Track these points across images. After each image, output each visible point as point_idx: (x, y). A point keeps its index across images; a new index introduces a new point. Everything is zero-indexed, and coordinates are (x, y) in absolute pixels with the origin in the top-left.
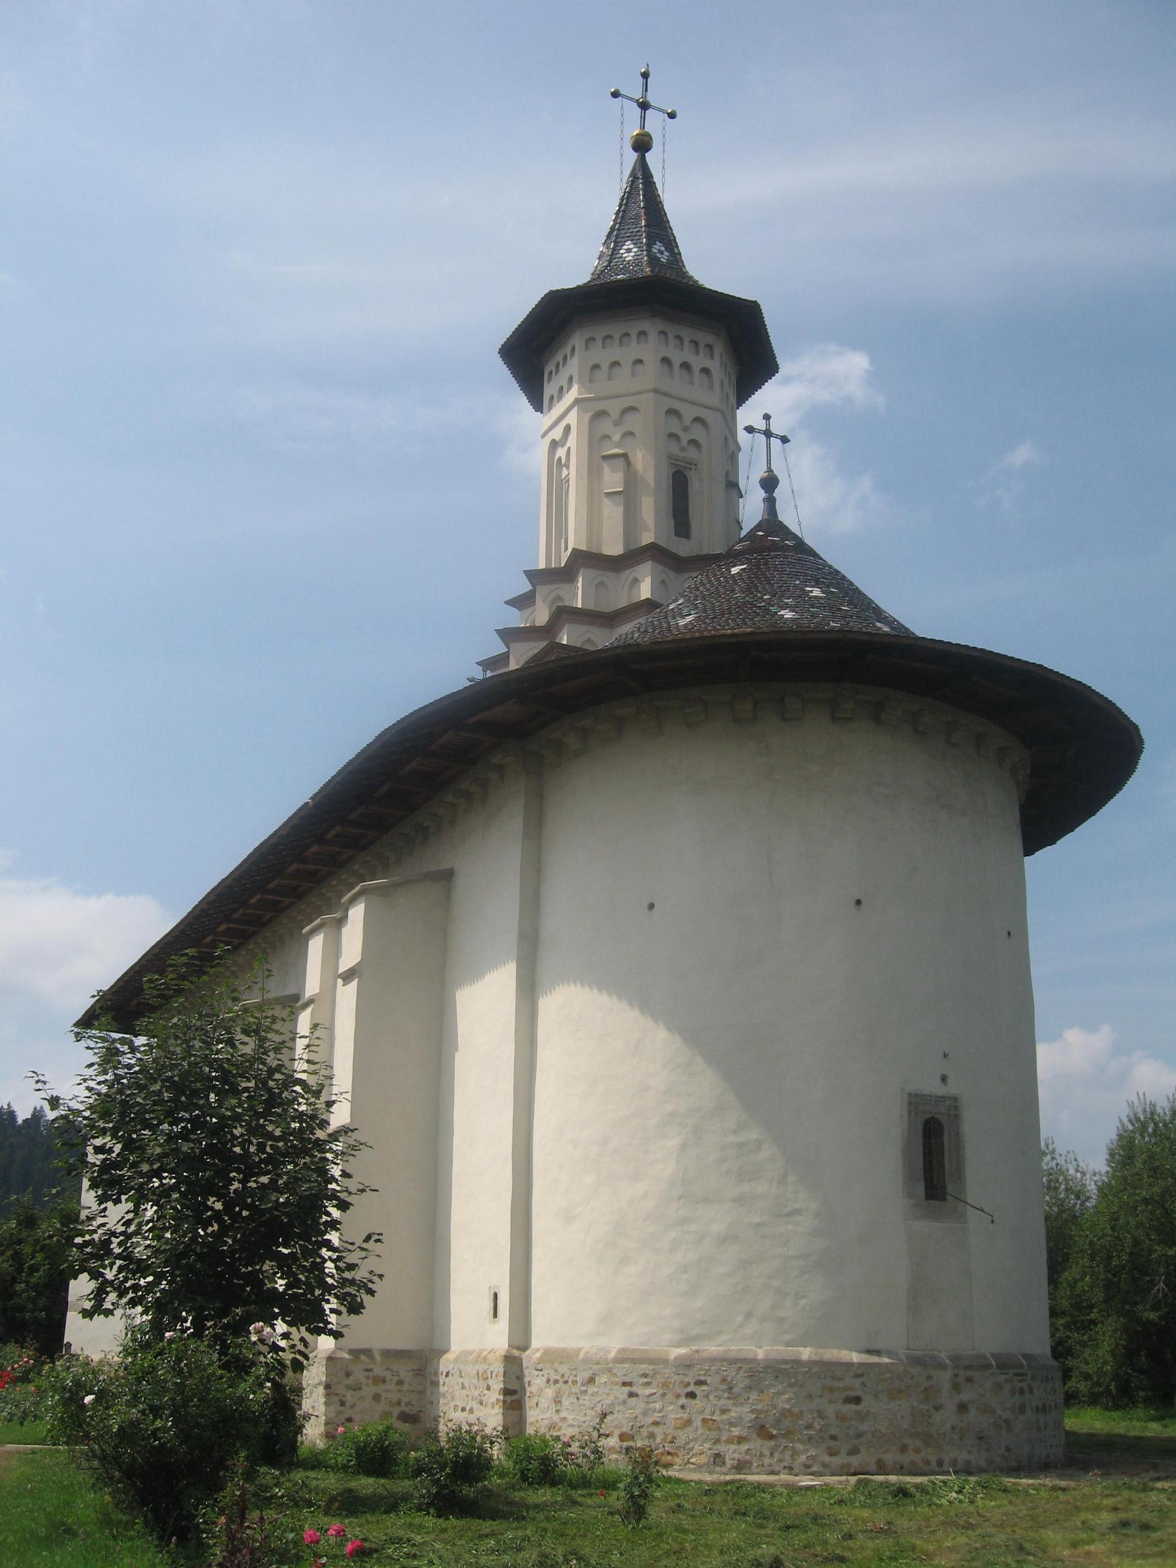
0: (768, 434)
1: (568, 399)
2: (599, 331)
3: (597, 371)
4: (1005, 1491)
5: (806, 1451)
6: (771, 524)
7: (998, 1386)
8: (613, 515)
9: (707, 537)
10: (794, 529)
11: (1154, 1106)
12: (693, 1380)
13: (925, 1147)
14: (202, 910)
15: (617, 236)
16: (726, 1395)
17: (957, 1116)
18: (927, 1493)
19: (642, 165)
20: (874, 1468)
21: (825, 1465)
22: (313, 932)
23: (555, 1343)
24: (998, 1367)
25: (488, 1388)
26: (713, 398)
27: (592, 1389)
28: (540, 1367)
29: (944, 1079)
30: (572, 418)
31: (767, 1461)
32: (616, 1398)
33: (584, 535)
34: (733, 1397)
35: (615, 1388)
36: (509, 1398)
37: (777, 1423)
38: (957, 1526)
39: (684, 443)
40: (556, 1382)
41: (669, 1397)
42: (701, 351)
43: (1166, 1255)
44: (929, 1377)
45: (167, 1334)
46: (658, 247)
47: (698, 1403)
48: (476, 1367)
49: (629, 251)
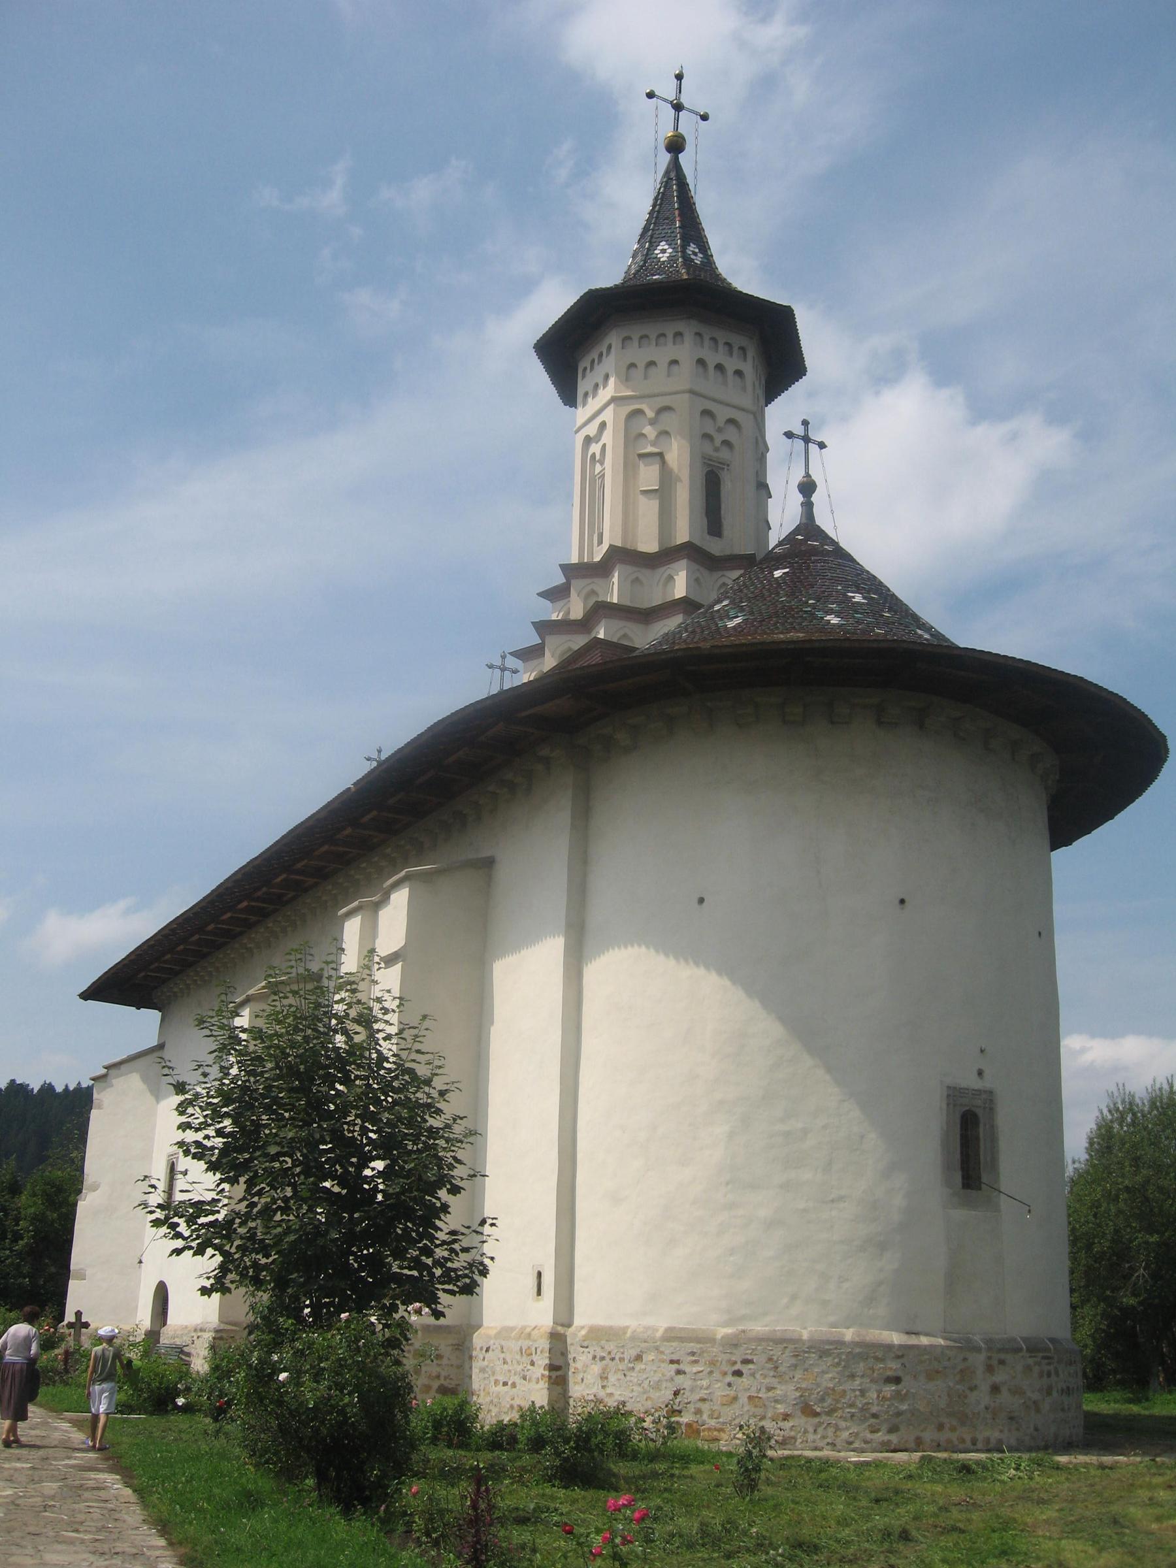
0: (807, 439)
1: (604, 396)
2: (636, 331)
3: (633, 370)
4: (1058, 1468)
5: (847, 1428)
6: (808, 527)
7: (1028, 1368)
8: (648, 510)
9: (736, 540)
10: (831, 533)
11: (1133, 1096)
12: (740, 1358)
13: (962, 1135)
14: (227, 889)
15: (652, 236)
16: (772, 1373)
17: (991, 1109)
18: (988, 1470)
19: (675, 166)
20: (912, 1445)
21: (866, 1442)
22: (349, 915)
23: (600, 1321)
24: (1028, 1350)
25: (532, 1363)
26: (746, 401)
27: (639, 1366)
28: (585, 1344)
29: (980, 1073)
30: (608, 415)
31: (811, 1437)
32: (663, 1375)
33: (619, 529)
34: (780, 1376)
35: (663, 1365)
36: (554, 1374)
37: (822, 1400)
38: (1032, 1500)
39: (718, 442)
40: (603, 1358)
41: (716, 1375)
42: (721, 347)
43: (1147, 1243)
44: (965, 1359)
45: (343, 1316)
46: (692, 247)
47: (745, 1381)
48: (520, 1343)
49: (663, 251)
